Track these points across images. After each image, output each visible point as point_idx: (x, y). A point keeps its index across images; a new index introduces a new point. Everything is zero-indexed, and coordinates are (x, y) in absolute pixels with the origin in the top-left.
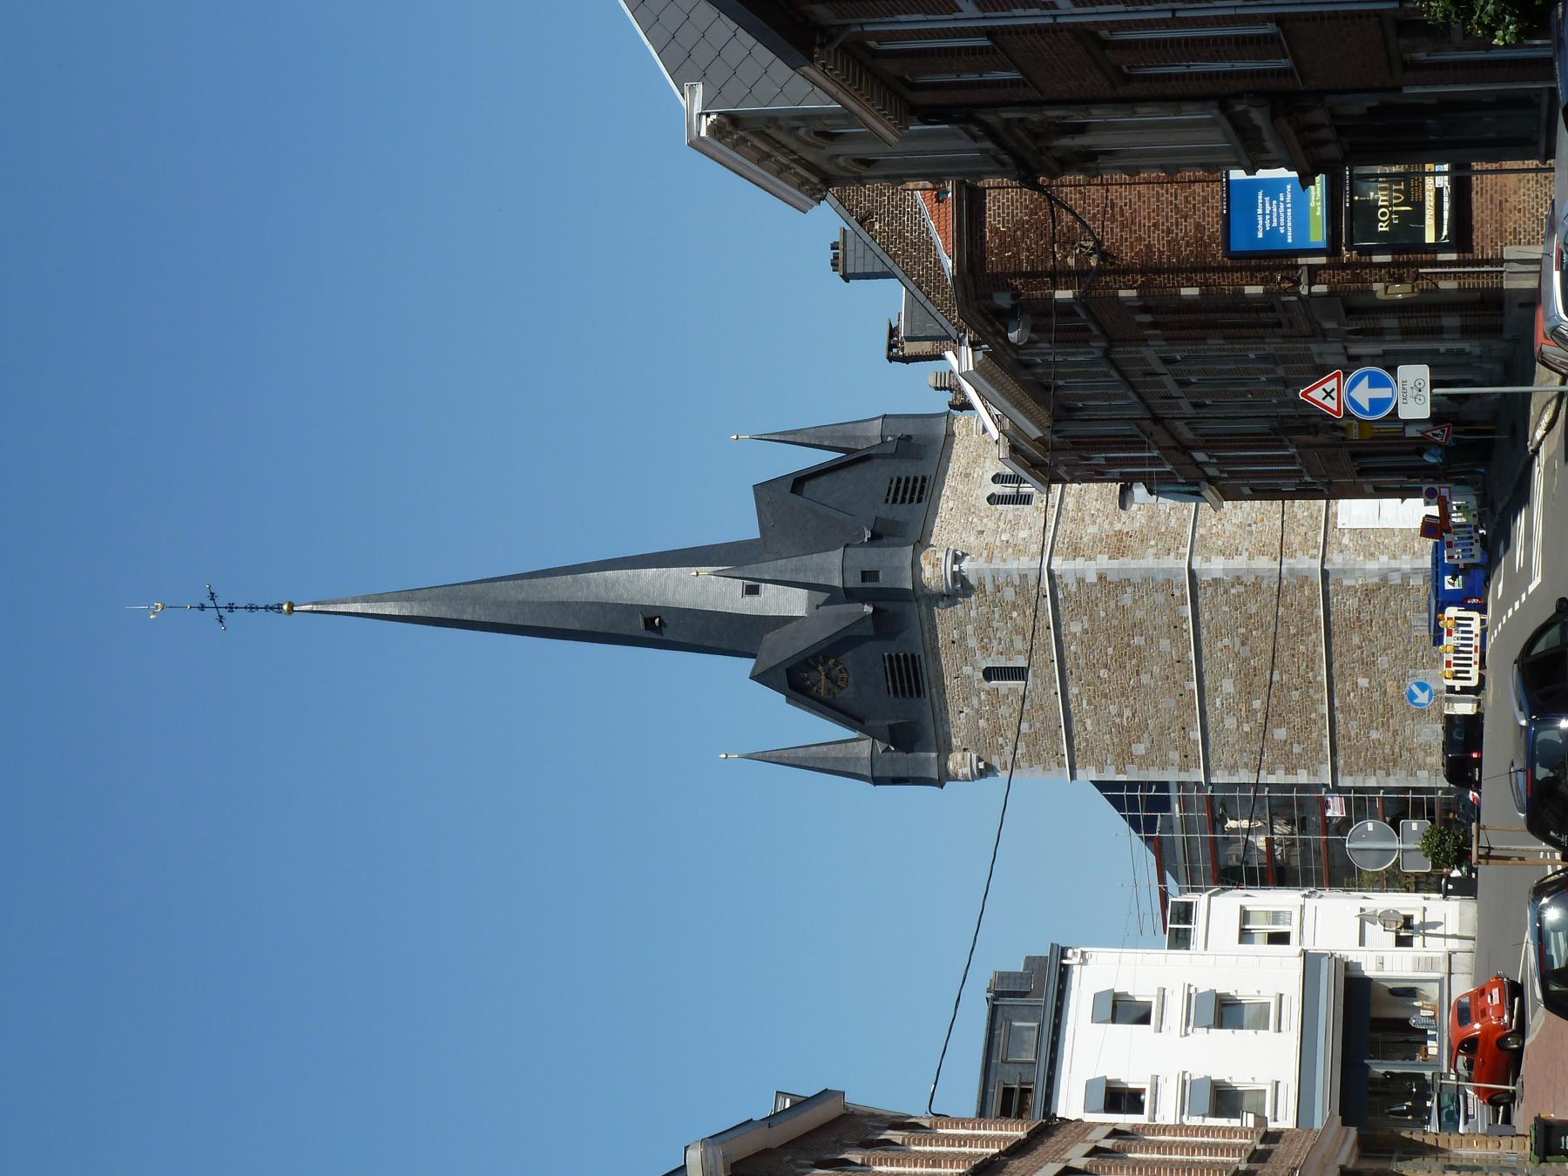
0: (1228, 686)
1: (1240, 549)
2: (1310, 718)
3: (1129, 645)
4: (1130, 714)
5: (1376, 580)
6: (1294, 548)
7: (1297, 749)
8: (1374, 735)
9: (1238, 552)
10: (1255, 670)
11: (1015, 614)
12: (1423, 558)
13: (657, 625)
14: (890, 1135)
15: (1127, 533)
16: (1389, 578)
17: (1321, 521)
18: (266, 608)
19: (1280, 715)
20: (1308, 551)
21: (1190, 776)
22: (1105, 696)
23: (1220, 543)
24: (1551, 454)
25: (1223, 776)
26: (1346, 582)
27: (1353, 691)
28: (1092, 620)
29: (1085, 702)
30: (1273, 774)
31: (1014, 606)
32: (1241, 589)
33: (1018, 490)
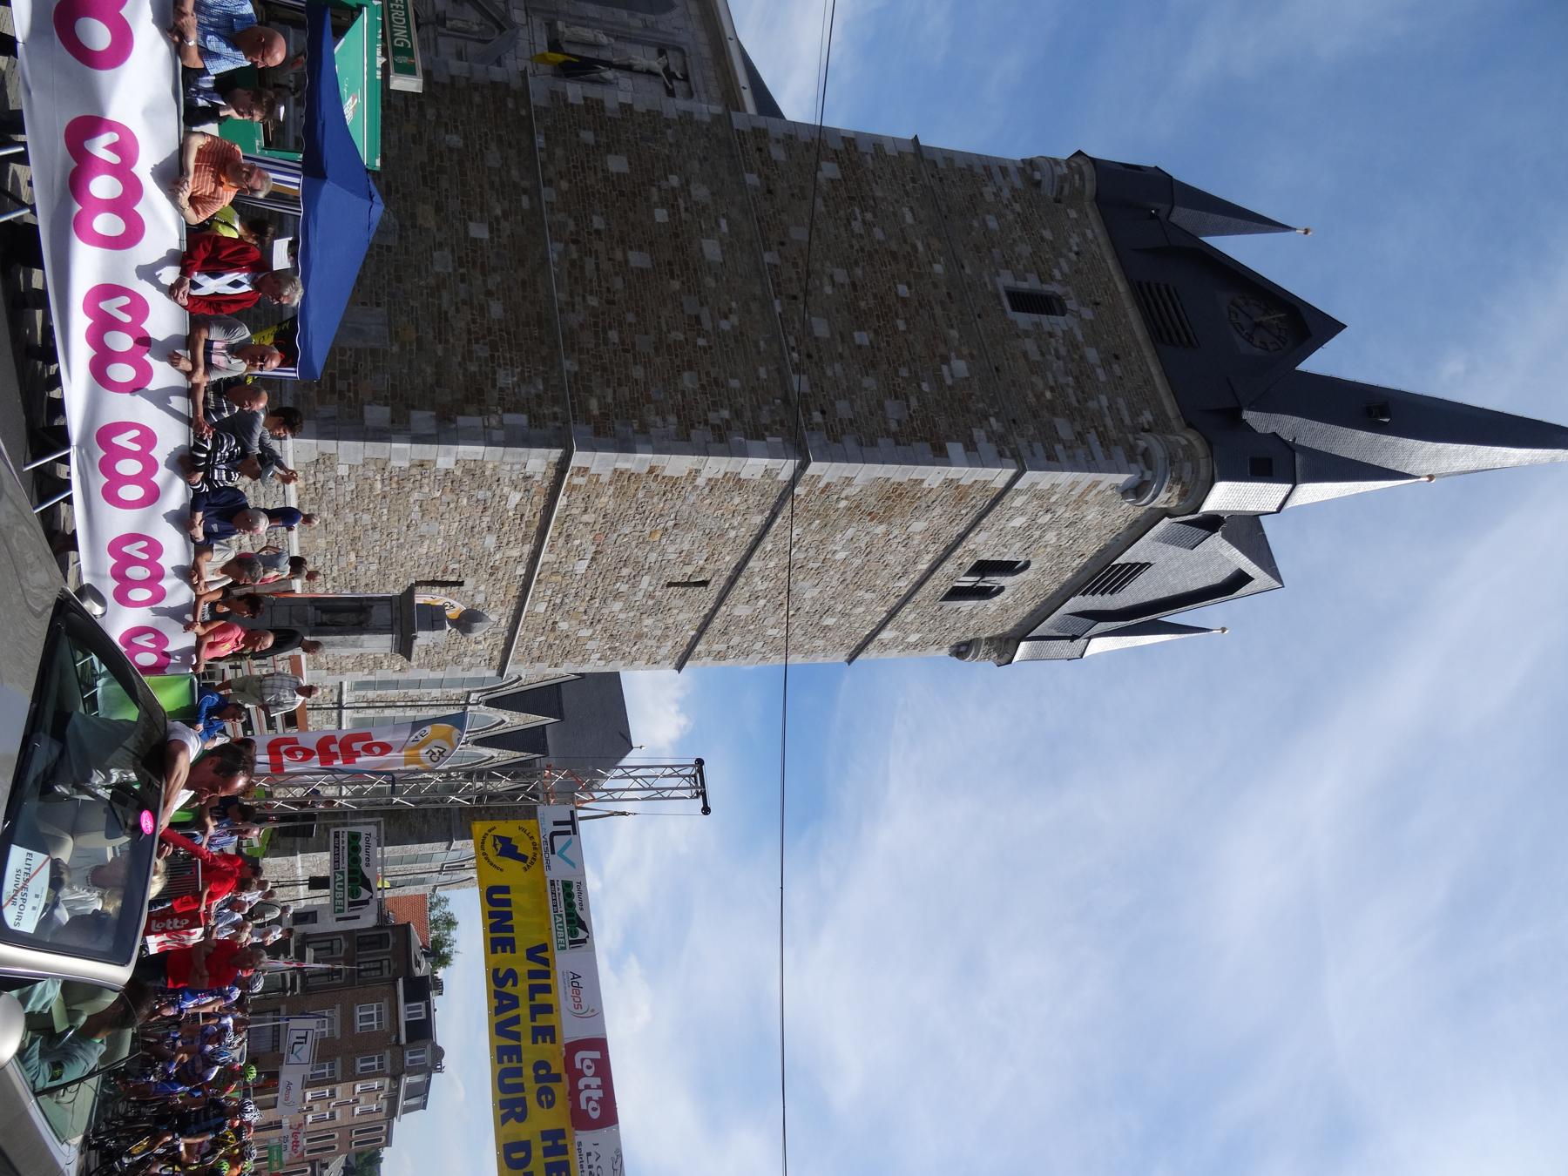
1: (707, 489)
2: (570, 182)
3: (876, 332)
4: (853, 223)
5: (462, 421)
6: (612, 488)
8: (455, 140)
9: (712, 484)
10: (672, 271)
11: (1048, 395)
12: (364, 459)
13: (264, 395)
14: (609, 74)
15: (872, 520)
16: (433, 422)
17: (555, 528)
19: (622, 194)
20: (590, 481)
22: (894, 255)
23: (737, 500)
24: (205, 276)
25: (701, 113)
26: (522, 419)
27: (497, 219)
28: (939, 379)
29: (921, 248)
30: (622, 105)
31: (1051, 408)
32: (713, 417)
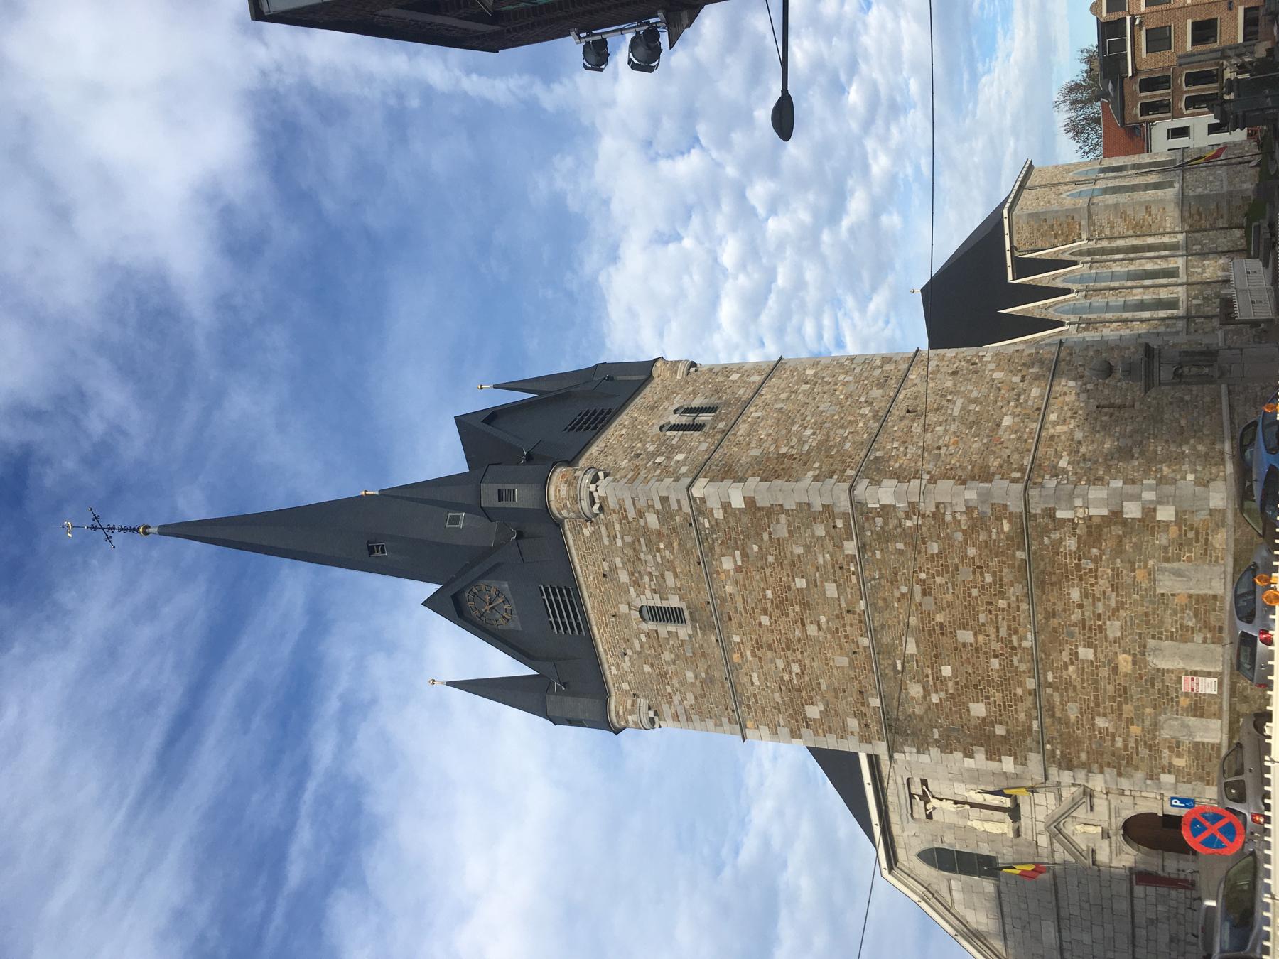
33: (694, 420)
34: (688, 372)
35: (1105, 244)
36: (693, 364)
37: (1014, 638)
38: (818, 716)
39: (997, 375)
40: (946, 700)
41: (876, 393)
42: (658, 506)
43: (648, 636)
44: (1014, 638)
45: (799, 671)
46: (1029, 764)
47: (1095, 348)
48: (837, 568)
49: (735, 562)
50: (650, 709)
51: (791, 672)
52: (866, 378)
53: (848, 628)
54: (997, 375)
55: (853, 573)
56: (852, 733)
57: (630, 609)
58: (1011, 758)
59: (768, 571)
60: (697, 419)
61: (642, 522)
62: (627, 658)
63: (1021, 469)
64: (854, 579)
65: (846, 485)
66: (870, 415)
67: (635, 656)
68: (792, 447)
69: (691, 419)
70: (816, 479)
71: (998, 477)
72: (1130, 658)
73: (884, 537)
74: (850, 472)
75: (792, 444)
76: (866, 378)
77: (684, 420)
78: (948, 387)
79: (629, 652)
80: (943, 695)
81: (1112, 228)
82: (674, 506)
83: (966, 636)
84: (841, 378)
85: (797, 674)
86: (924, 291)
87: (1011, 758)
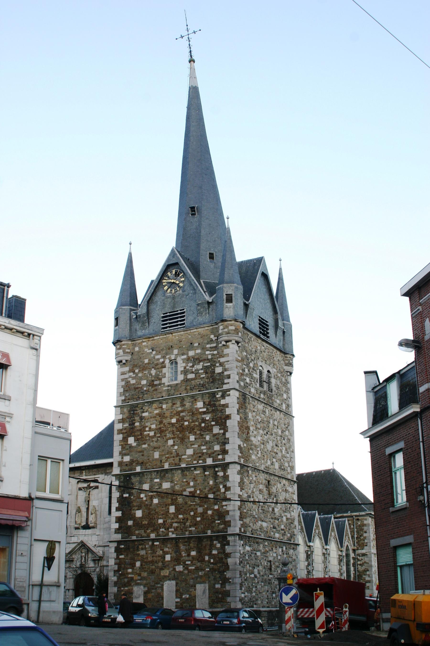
0: (166, 485)
7: (130, 523)
18: (190, 51)
21: (116, 467)
33: (264, 381)
34: (287, 372)
35: (352, 561)
36: (291, 374)
37: (173, 530)
38: (129, 443)
39: (284, 519)
40: (142, 501)
41: (277, 466)
42: (226, 373)
43: (163, 362)
44: (173, 530)
45: (150, 435)
46: (116, 535)
47: (296, 559)
48: (200, 455)
49: (201, 408)
50: (126, 361)
51: (149, 431)
52: (284, 460)
53: (173, 458)
54: (284, 519)
55: (198, 462)
56: (122, 458)
57: (176, 355)
58: (118, 527)
59: (197, 423)
60: (265, 383)
61: (218, 365)
62: (151, 351)
63: (245, 532)
64: (195, 462)
65: (237, 460)
66: (267, 465)
67: (152, 356)
68: (253, 432)
69: (265, 380)
70: (239, 446)
71: (242, 522)
72: (167, 574)
73: (215, 476)
74: (242, 460)
75: (254, 432)
76: (284, 460)
77: (265, 376)
78: (279, 498)
79: (154, 352)
80: (145, 499)
81: (360, 565)
82: (226, 381)
83: (172, 509)
84: (284, 448)
85: (149, 434)
86: (334, 471)
87: (118, 527)
